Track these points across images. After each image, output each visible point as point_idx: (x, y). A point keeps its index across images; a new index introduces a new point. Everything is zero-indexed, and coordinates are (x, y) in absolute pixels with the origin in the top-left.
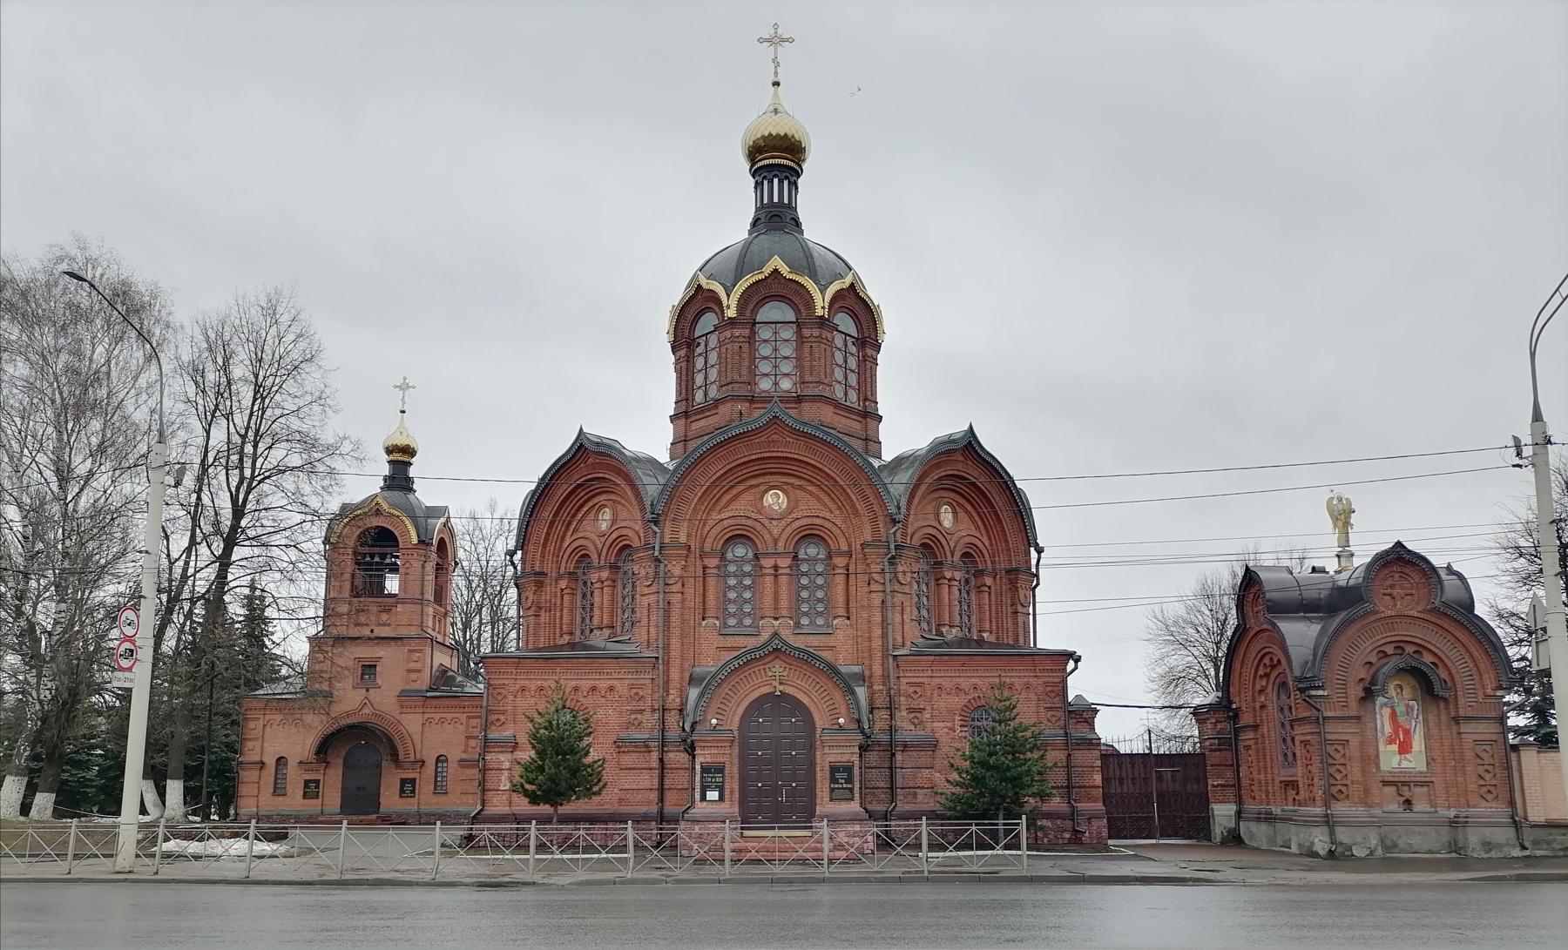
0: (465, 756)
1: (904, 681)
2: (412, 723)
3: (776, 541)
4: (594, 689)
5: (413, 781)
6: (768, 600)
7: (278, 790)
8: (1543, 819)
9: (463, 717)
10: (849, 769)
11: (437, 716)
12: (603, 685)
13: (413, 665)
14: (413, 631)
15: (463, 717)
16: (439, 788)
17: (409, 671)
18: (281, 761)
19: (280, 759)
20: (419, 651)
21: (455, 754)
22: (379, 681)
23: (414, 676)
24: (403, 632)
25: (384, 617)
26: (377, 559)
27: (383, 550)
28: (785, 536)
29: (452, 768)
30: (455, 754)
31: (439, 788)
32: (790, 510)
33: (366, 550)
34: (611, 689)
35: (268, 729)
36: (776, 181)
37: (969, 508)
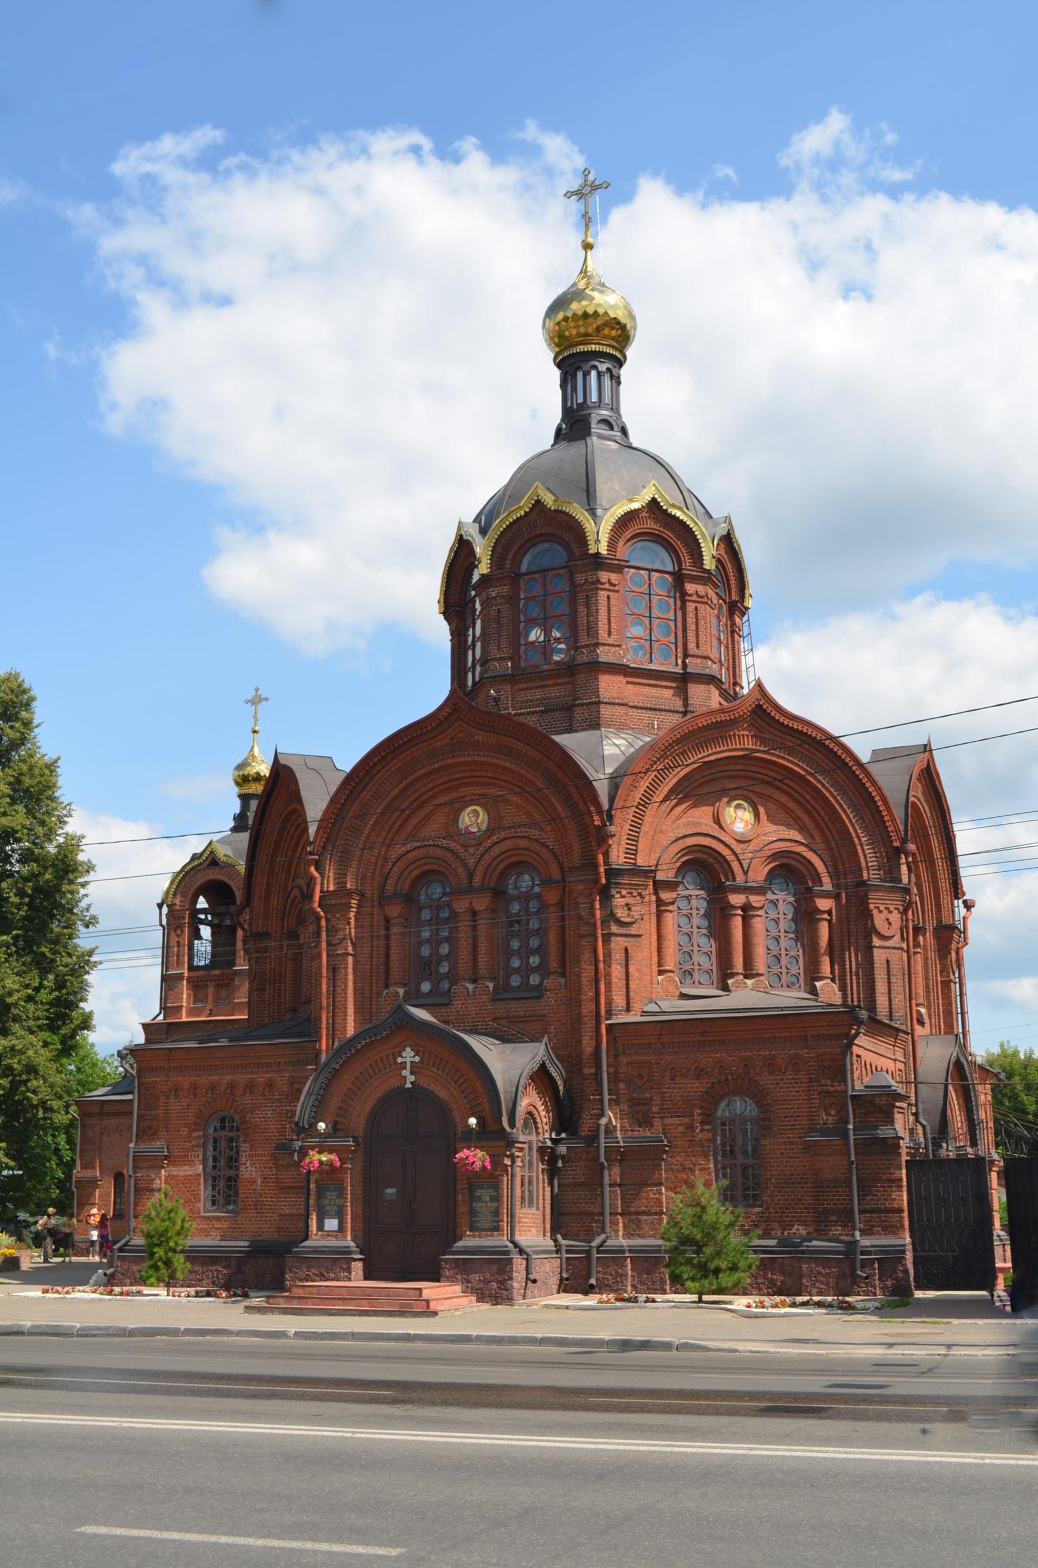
1: (624, 1060)
3: (471, 875)
4: (251, 1086)
6: (464, 956)
12: (261, 1079)
28: (481, 868)
32: (490, 831)
34: (270, 1084)
36: (594, 373)
37: (784, 799)
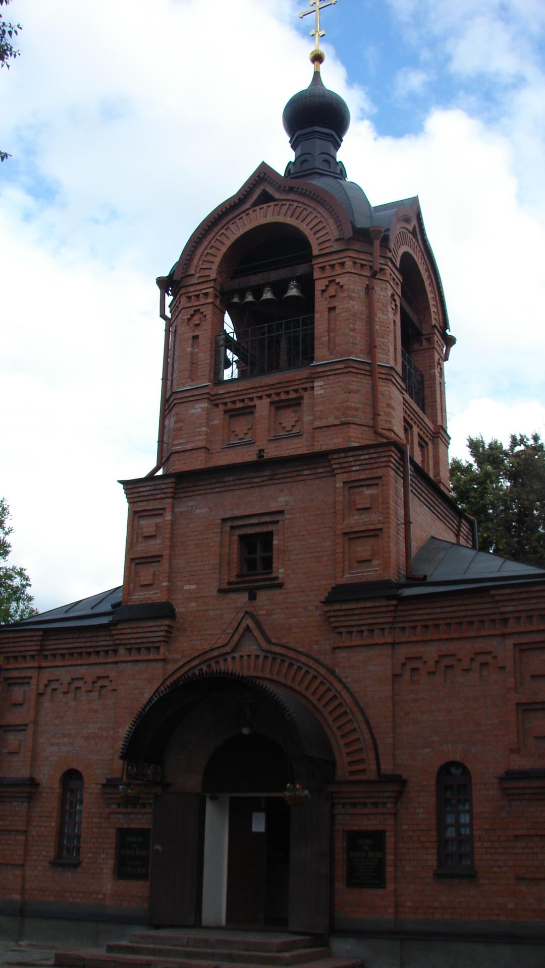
0: (519, 763)
2: (366, 672)
5: (378, 838)
7: (66, 856)
8: (411, 520)
9: (504, 649)
10: (355, 879)
11: (431, 652)
13: (357, 521)
14: (357, 437)
15: (504, 649)
16: (455, 863)
17: (352, 536)
18: (71, 778)
19: (445, 769)
20: (374, 482)
21: (487, 763)
22: (280, 571)
23: (363, 549)
24: (327, 442)
25: (288, 418)
26: (268, 295)
27: (274, 276)
29: (485, 794)
30: (487, 763)
31: (455, 863)
33: (237, 283)
35: (46, 704)
